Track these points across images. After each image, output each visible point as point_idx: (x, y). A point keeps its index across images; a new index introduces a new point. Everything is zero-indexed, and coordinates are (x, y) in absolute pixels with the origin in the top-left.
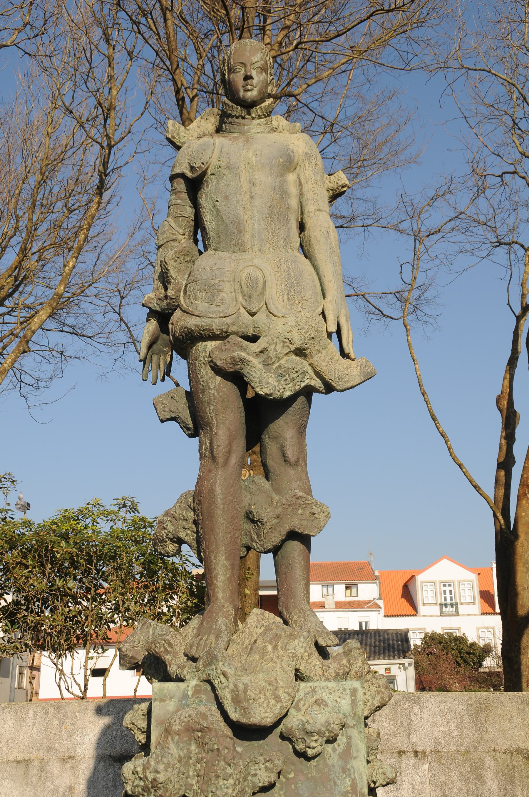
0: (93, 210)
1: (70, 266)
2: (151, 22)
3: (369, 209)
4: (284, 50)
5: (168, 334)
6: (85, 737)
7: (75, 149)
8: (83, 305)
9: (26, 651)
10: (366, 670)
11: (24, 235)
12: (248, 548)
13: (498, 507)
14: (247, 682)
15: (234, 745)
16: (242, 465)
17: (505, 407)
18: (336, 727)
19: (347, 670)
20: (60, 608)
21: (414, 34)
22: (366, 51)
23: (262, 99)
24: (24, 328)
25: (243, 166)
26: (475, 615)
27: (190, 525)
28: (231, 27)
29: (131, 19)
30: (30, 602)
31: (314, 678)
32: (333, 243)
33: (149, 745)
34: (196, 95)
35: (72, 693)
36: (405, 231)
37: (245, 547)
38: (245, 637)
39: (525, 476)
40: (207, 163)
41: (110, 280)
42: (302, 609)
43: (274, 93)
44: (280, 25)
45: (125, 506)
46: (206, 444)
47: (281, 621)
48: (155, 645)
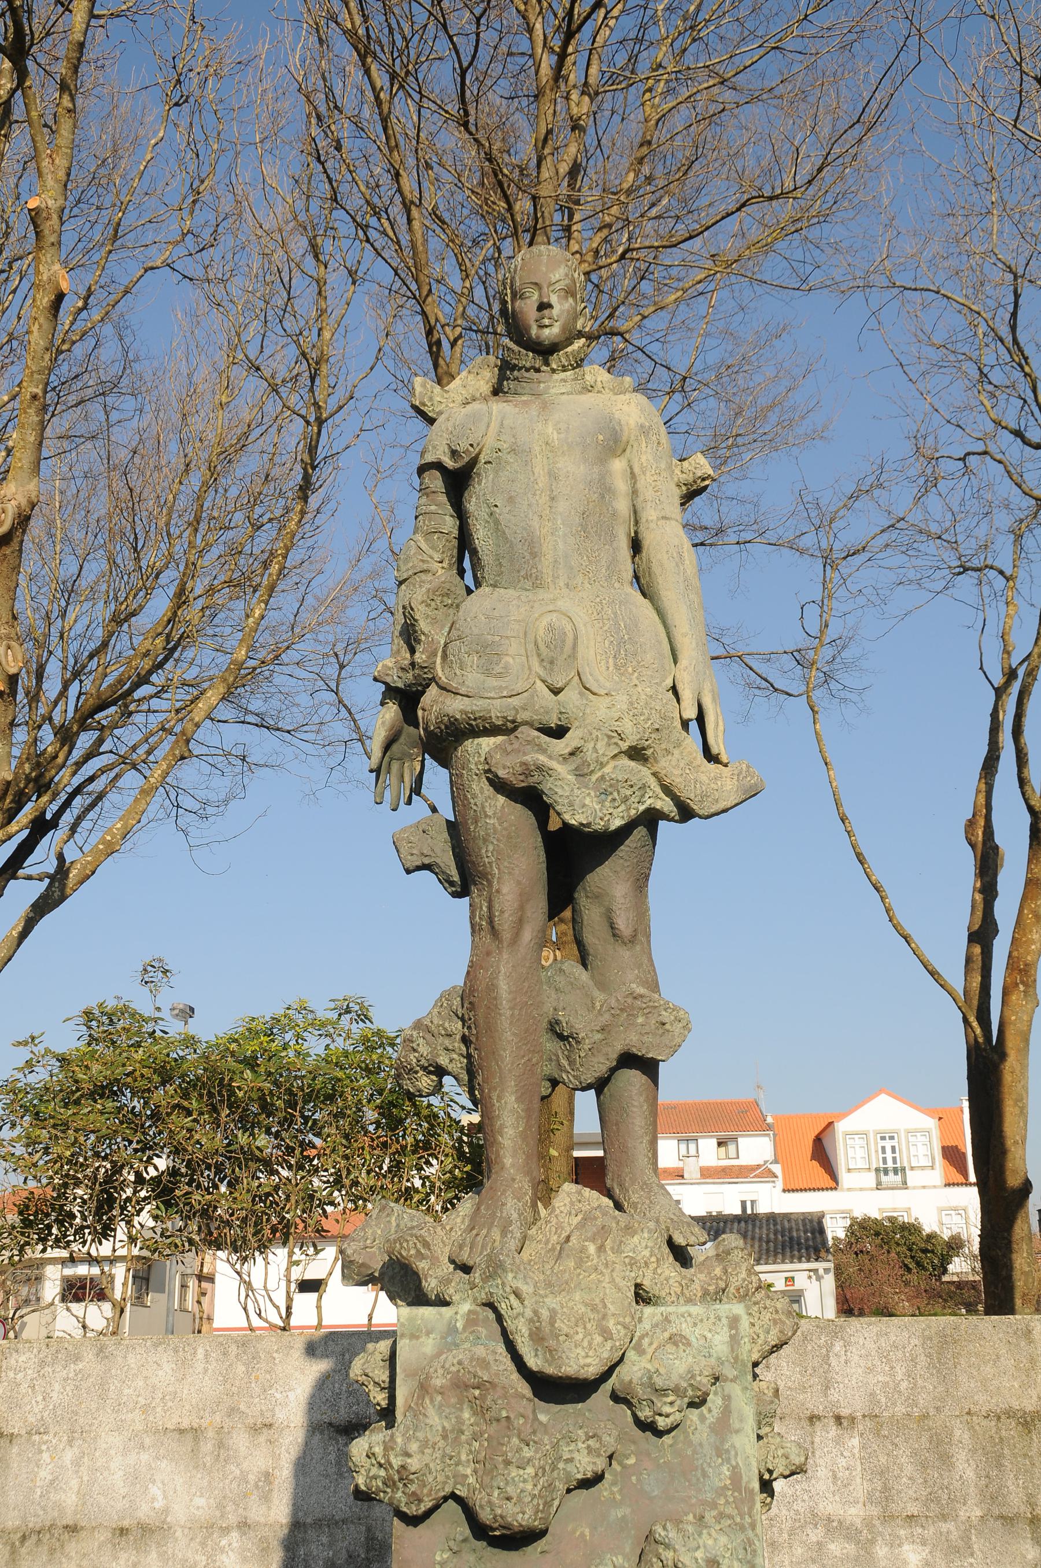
0: (292, 525)
1: (256, 615)
2: (386, 224)
3: (748, 516)
4: (603, 261)
5: (417, 726)
6: (289, 1394)
7: (264, 428)
8: (278, 679)
9: (190, 1250)
10: (754, 1285)
11: (182, 568)
12: (554, 1083)
13: (970, 1007)
14: (554, 1305)
15: (534, 1411)
16: (543, 942)
17: (980, 839)
18: (705, 1381)
19: (722, 1285)
20: (245, 1181)
21: (814, 233)
22: (736, 261)
23: (567, 339)
24: (182, 719)
25: (537, 449)
26: (935, 1187)
27: (456, 1045)
28: (515, 228)
29: (354, 220)
30: (194, 1171)
31: (668, 1298)
32: (689, 572)
33: (394, 1411)
34: (460, 336)
35: (266, 1321)
36: (807, 549)
37: (549, 1080)
38: (550, 1231)
39: (1015, 954)
40: (478, 445)
41: (321, 637)
42: (645, 1183)
43: (587, 329)
44: (596, 223)
45: (348, 1011)
46: (481, 908)
47: (611, 1204)
48: (401, 1244)
